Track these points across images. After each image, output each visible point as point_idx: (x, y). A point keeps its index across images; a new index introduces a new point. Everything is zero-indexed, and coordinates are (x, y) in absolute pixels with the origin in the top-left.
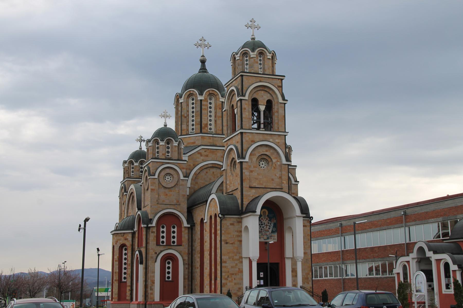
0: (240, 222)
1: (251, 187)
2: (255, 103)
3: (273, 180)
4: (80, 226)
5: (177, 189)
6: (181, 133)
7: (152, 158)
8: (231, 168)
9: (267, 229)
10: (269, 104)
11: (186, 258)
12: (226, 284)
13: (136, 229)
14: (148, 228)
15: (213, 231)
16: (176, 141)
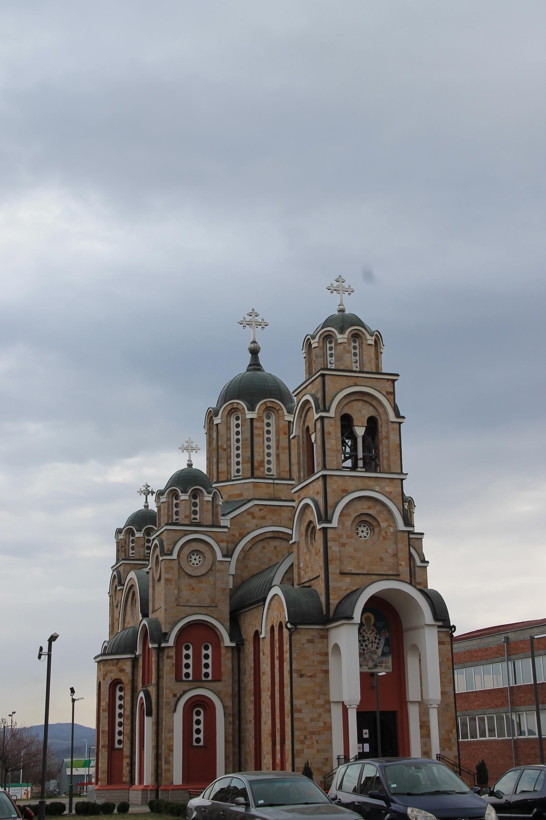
0: (325, 637)
1: (342, 574)
2: (347, 422)
3: (381, 559)
4: (41, 649)
5: (211, 579)
8: (306, 540)
9: (374, 649)
10: (372, 425)
11: (229, 704)
15: (277, 654)
16: (209, 493)
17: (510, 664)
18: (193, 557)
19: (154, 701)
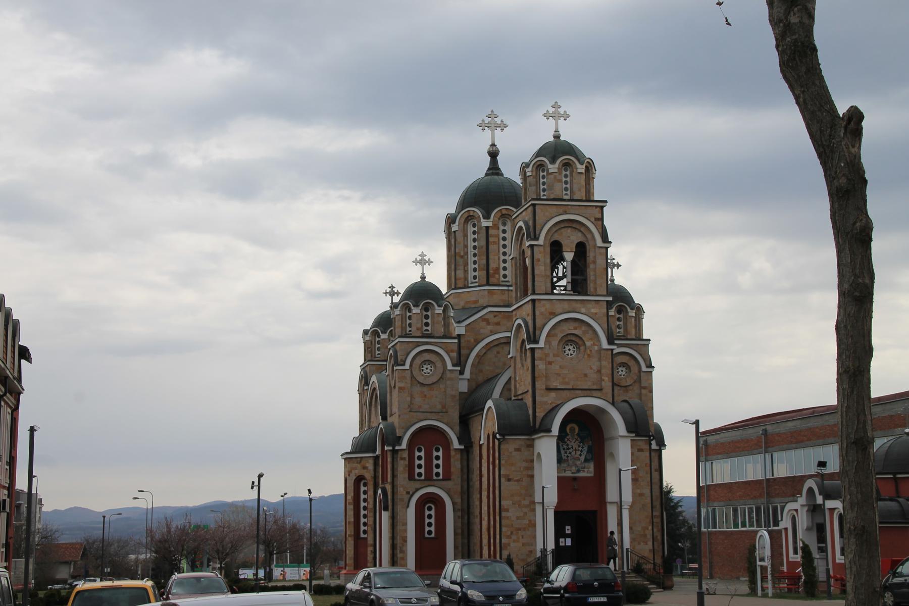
0: (531, 446)
1: (549, 389)
3: (586, 375)
4: (253, 483)
5: (442, 386)
6: (456, 284)
7: (400, 337)
8: (521, 356)
9: (577, 455)
10: (581, 249)
11: (459, 500)
12: (509, 544)
13: (378, 452)
14: (395, 452)
16: (439, 306)
17: (768, 456)
18: (425, 367)
19: (390, 497)
